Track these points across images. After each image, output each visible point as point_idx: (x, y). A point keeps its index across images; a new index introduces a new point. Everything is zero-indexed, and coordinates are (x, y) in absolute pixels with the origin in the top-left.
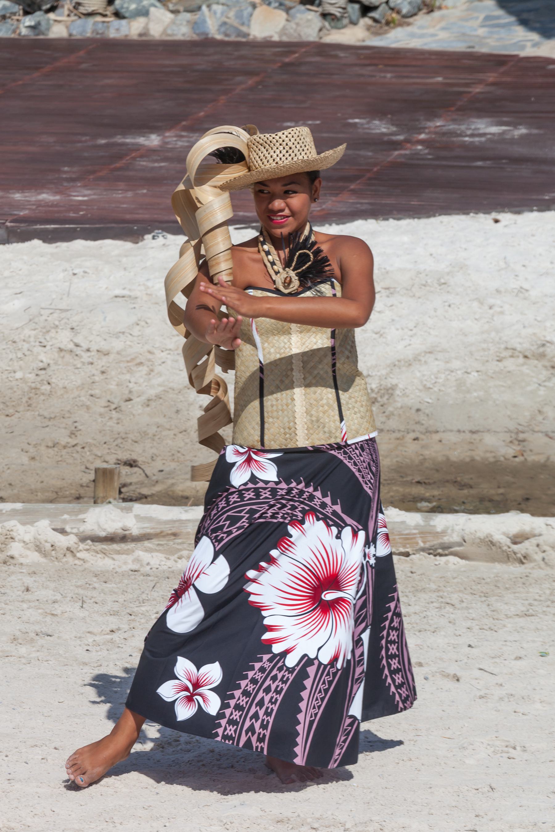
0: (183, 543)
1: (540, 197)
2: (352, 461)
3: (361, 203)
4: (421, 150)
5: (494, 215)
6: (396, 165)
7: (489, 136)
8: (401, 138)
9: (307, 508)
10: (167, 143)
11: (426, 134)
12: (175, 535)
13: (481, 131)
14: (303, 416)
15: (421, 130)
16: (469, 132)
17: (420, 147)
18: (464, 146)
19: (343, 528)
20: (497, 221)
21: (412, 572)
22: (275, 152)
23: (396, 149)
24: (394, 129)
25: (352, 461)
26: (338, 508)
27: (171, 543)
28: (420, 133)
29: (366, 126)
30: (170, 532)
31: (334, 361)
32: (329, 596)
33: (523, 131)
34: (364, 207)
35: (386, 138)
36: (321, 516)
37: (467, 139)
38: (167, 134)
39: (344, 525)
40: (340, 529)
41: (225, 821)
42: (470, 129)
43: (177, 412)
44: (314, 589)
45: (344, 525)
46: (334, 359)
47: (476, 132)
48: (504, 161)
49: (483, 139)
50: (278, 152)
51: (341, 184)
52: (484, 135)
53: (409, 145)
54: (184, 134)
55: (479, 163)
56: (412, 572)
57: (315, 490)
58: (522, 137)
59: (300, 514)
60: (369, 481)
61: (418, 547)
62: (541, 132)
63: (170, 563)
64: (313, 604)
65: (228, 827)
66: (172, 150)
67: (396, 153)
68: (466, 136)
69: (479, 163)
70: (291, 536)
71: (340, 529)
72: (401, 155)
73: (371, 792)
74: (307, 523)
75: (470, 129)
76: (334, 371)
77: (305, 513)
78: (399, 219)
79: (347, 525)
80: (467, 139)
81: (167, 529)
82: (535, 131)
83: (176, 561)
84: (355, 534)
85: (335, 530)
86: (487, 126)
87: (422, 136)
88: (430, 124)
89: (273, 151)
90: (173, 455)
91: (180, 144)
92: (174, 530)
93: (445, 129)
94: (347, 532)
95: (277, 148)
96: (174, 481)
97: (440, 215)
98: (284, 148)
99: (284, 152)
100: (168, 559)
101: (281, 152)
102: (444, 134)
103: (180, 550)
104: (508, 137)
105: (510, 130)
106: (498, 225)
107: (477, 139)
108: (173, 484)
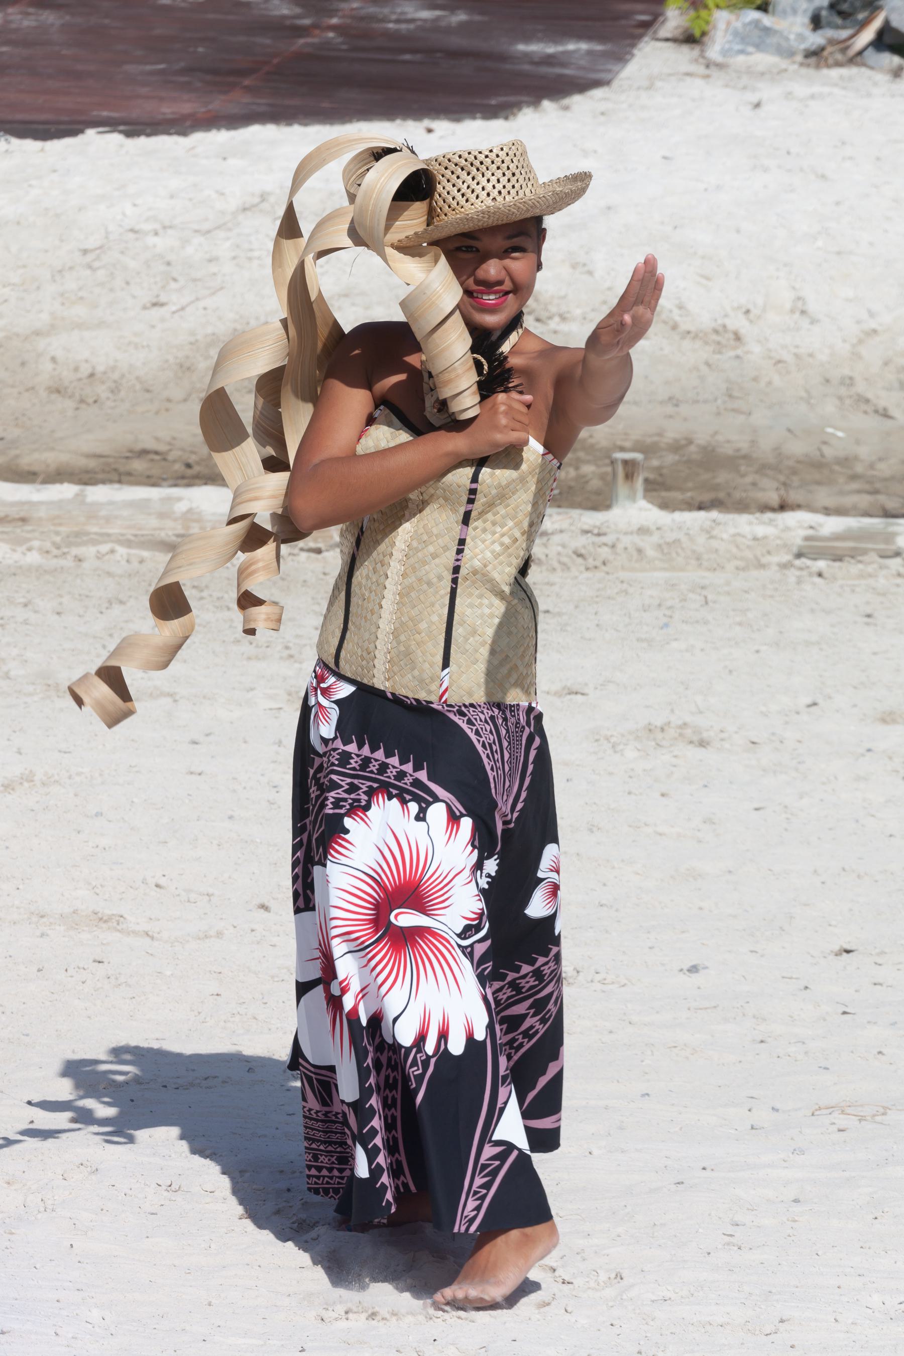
0: (33, 531)
1: (486, 102)
3: (258, 104)
4: (333, 38)
5: (427, 123)
6: (300, 57)
7: (419, 23)
8: (307, 22)
9: (375, 785)
10: (11, 22)
11: (340, 17)
12: (23, 520)
13: (409, 16)
14: (389, 638)
15: (332, 13)
16: (394, 17)
17: (331, 35)
18: (387, 34)
19: (429, 804)
20: (430, 131)
21: (325, 574)
22: (488, 181)
23: (300, 36)
24: (298, 10)
26: (423, 775)
27: (18, 530)
28: (331, 17)
29: (263, 6)
30: (17, 516)
33: (461, 17)
34: (262, 109)
35: (288, 22)
36: (394, 792)
37: (391, 25)
38: (10, 10)
39: (431, 800)
40: (424, 805)
41: (94, 884)
42: (395, 13)
43: (23, 364)
44: (377, 906)
45: (431, 800)
47: (403, 17)
48: (439, 55)
49: (412, 26)
50: (494, 179)
51: (231, 79)
52: (413, 21)
53: (317, 32)
54: (31, 10)
55: (407, 57)
56: (325, 574)
58: (462, 25)
59: (364, 797)
61: (332, 542)
62: (485, 18)
63: (17, 556)
65: (98, 891)
66: (17, 30)
67: (302, 41)
68: (390, 21)
69: (407, 57)
71: (424, 805)
72: (307, 44)
73: (278, 850)
74: (374, 807)
75: (395, 13)
77: (371, 793)
78: (306, 125)
79: (437, 799)
80: (391, 25)
81: (14, 513)
82: (477, 18)
83: (24, 554)
84: (453, 819)
85: (414, 807)
86: (416, 10)
87: (335, 21)
88: (343, 5)
89: (485, 179)
90: (17, 419)
91: (26, 23)
92: (22, 514)
93: (363, 12)
94: (437, 812)
95: (493, 175)
96: (17, 452)
97: (358, 120)
98: (504, 175)
99: (504, 180)
100: (14, 550)
101: (498, 181)
102: (362, 19)
103: (29, 540)
104: (443, 24)
105: (445, 16)
106: (431, 135)
107: (403, 26)
108: (17, 457)
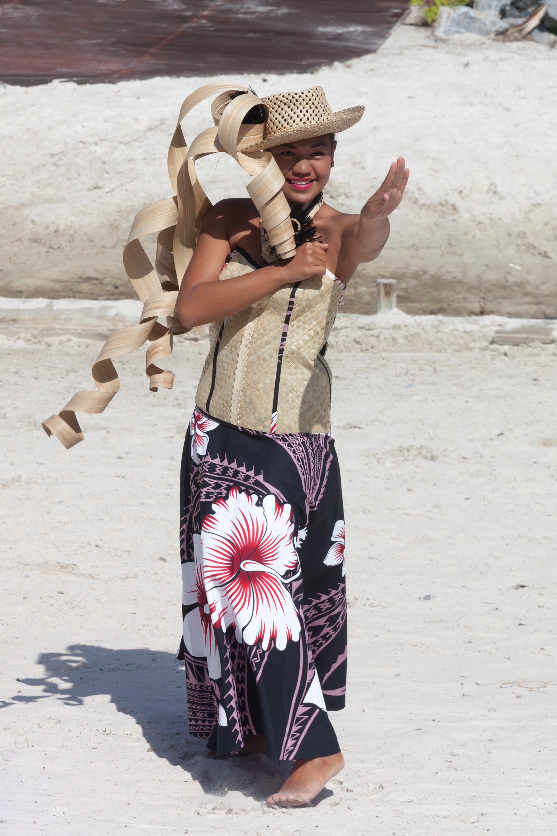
0: (20, 327)
1: (299, 63)
2: (292, 449)
3: (159, 64)
4: (205, 24)
5: (263, 76)
6: (185, 35)
7: (258, 14)
8: (189, 13)
9: (231, 484)
11: (210, 11)
12: (14, 321)
13: (252, 10)
15: (205, 8)
16: (243, 11)
17: (204, 21)
18: (239, 21)
19: (264, 496)
20: (265, 81)
21: (200, 354)
23: (185, 22)
24: (184, 6)
25: (292, 449)
26: (260, 478)
27: (11, 327)
28: (204, 10)
29: (162, 4)
30: (11, 318)
31: (282, 347)
32: (250, 566)
33: (284, 10)
34: (162, 67)
35: (177, 14)
36: (243, 488)
37: (241, 16)
39: (266, 493)
40: (261, 497)
41: (58, 545)
42: (243, 8)
43: (14, 224)
44: (232, 559)
45: (266, 493)
46: (282, 345)
47: (248, 11)
48: (270, 34)
49: (254, 16)
51: (142, 49)
52: (254, 13)
53: (195, 20)
55: (251, 35)
56: (200, 354)
57: (239, 465)
58: (285, 16)
59: (224, 492)
60: (302, 459)
61: (205, 334)
62: (299, 11)
63: (10, 343)
64: (232, 574)
65: (60, 549)
67: (186, 25)
68: (240, 13)
69: (251, 35)
70: (214, 513)
71: (261, 497)
72: (189, 27)
73: (171, 524)
74: (230, 498)
75: (243, 8)
76: (280, 358)
77: (229, 489)
78: (188, 77)
79: (269, 493)
80: (241, 16)
81: (9, 316)
82: (294, 11)
83: (15, 342)
84: (279, 505)
85: (255, 498)
86: (257, 6)
87: (206, 13)
88: (212, 3)
90: (10, 258)
91: (16, 14)
92: (14, 317)
93: (224, 8)
94: (270, 501)
96: (11, 279)
97: (221, 74)
100: (9, 339)
102: (223, 11)
103: (18, 333)
104: (273, 15)
105: (274, 10)
106: (266, 83)
107: (249, 16)
108: (10, 281)
